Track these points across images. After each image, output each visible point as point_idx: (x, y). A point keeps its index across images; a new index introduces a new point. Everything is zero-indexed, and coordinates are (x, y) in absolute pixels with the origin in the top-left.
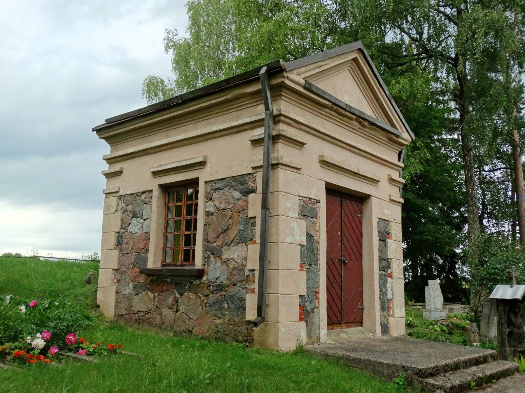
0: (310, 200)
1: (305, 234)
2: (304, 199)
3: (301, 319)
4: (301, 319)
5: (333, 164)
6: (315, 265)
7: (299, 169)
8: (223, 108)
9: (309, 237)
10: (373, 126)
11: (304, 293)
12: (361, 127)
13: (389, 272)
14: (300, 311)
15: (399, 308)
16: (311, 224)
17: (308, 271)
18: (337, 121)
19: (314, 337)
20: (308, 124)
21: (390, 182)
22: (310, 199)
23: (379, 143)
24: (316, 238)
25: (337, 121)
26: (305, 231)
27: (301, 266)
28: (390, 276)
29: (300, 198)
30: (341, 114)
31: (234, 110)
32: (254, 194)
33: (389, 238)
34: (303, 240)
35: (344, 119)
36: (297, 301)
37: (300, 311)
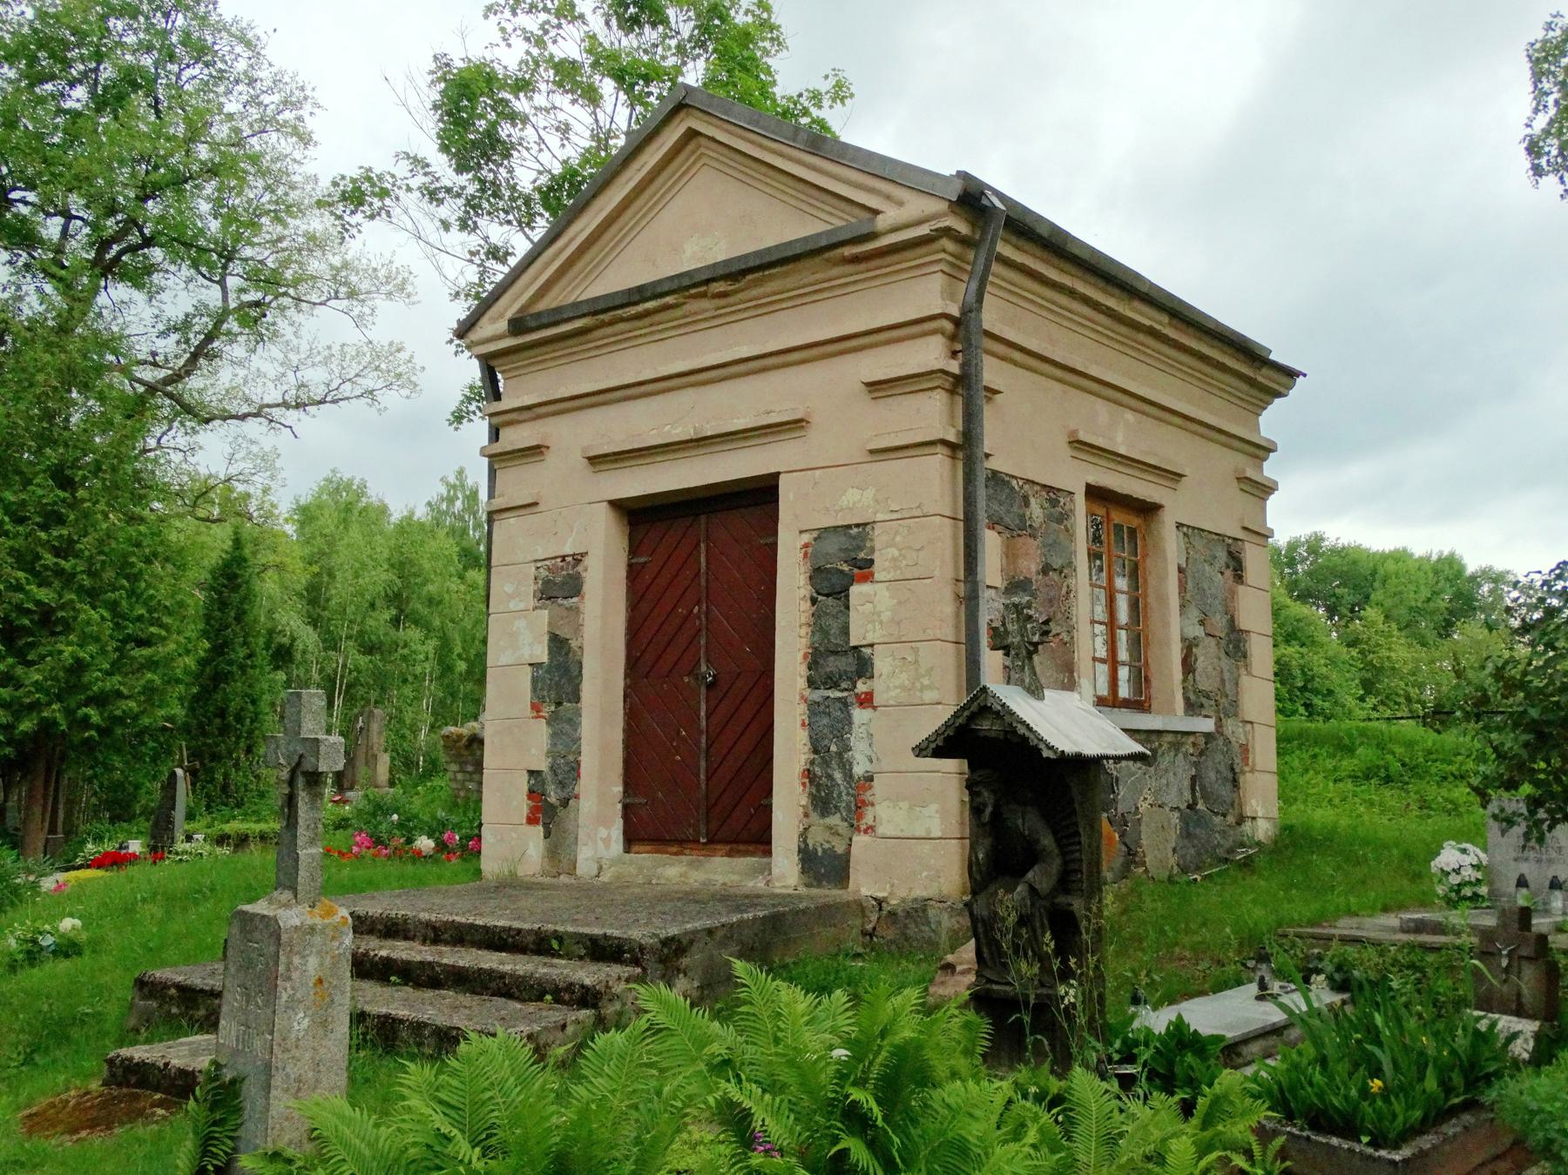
0: (563, 560)
1: (546, 638)
2: (547, 563)
3: (532, 820)
4: (532, 820)
5: (615, 454)
6: (569, 701)
7: (535, 504)
8: (547, 353)
9: (558, 644)
10: (749, 277)
11: (543, 765)
12: (722, 302)
13: (861, 687)
14: (532, 804)
15: (904, 805)
16: (565, 613)
17: (553, 720)
18: (645, 335)
19: (565, 861)
20: (544, 399)
21: (876, 395)
22: (563, 558)
23: (826, 295)
24: (574, 644)
25: (645, 335)
26: (546, 629)
27: (535, 707)
28: (867, 701)
29: (539, 564)
30: (639, 317)
31: (790, 304)
32: (525, 811)
33: (867, 578)
34: (542, 654)
35: (657, 318)
36: (523, 783)
37: (532, 804)
